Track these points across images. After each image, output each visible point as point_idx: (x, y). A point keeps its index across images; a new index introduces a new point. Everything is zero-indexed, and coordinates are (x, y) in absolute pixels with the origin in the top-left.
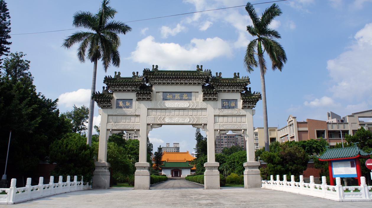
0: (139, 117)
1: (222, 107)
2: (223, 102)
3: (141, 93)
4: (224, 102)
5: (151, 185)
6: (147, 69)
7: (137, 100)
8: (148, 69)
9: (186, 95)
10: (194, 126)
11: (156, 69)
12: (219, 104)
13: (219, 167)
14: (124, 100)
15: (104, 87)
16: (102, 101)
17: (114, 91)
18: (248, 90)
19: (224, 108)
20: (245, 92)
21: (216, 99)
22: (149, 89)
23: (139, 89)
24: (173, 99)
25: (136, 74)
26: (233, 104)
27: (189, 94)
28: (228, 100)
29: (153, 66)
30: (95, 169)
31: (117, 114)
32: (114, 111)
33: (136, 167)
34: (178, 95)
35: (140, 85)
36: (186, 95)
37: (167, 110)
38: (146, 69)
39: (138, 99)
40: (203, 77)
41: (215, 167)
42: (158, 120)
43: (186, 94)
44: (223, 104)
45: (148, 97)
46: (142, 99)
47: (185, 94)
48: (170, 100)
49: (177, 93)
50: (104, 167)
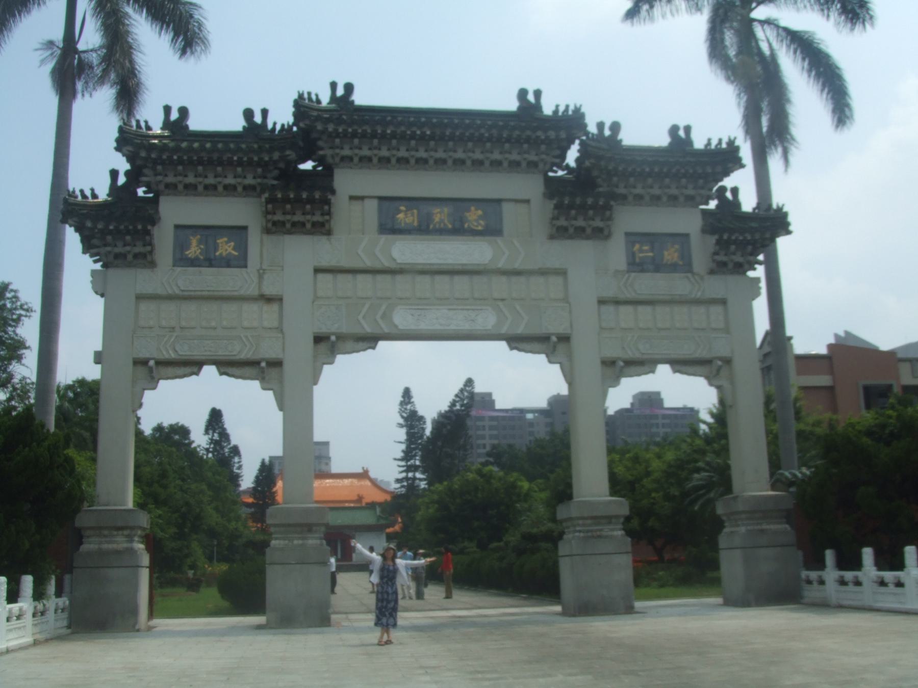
0: (275, 307)
1: (629, 264)
3: (286, 200)
4: (637, 247)
6: (309, 94)
7: (267, 231)
8: (314, 98)
10: (514, 345)
11: (343, 101)
12: (616, 252)
13: (628, 519)
15: (114, 174)
16: (110, 232)
17: (162, 187)
18: (729, 195)
20: (717, 206)
21: (606, 232)
22: (322, 181)
23: (275, 182)
24: (424, 229)
25: (258, 119)
26: (671, 255)
28: (651, 238)
29: (334, 85)
30: (81, 543)
31: (177, 292)
32: (165, 276)
34: (446, 210)
37: (399, 278)
38: (306, 96)
39: (270, 225)
40: (552, 134)
42: (364, 317)
43: (476, 210)
44: (633, 254)
46: (288, 226)
47: (473, 208)
50: (126, 532)
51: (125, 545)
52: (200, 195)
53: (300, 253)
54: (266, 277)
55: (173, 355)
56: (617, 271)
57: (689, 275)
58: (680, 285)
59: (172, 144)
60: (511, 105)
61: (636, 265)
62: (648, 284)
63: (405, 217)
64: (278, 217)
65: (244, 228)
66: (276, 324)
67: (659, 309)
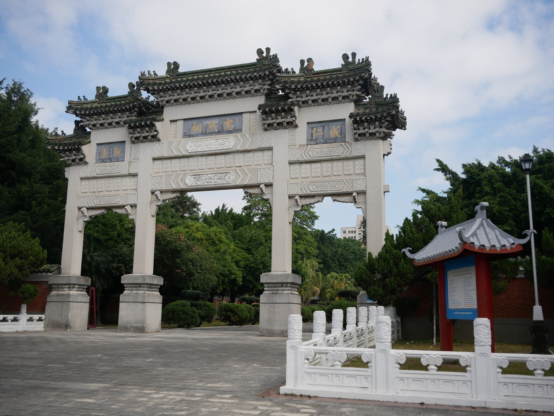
1: (308, 140)
2: (312, 128)
4: (315, 129)
5: (144, 324)
7: (133, 142)
9: (232, 121)
12: (301, 134)
14: (111, 145)
19: (312, 142)
25: (350, 60)
27: (237, 118)
33: (123, 284)
35: (361, 82)
36: (232, 121)
41: (150, 286)
42: (181, 180)
44: (312, 134)
45: (289, 119)
48: (197, 135)
49: (212, 118)
51: (67, 292)
52: (320, 105)
53: (148, 150)
54: (131, 165)
55: (93, 205)
56: (300, 145)
57: (343, 143)
58: (337, 150)
59: (99, 105)
60: (253, 58)
61: (312, 140)
62: (317, 151)
63: (197, 128)
64: (270, 121)
65: (124, 142)
66: (362, 171)
67: (325, 164)
